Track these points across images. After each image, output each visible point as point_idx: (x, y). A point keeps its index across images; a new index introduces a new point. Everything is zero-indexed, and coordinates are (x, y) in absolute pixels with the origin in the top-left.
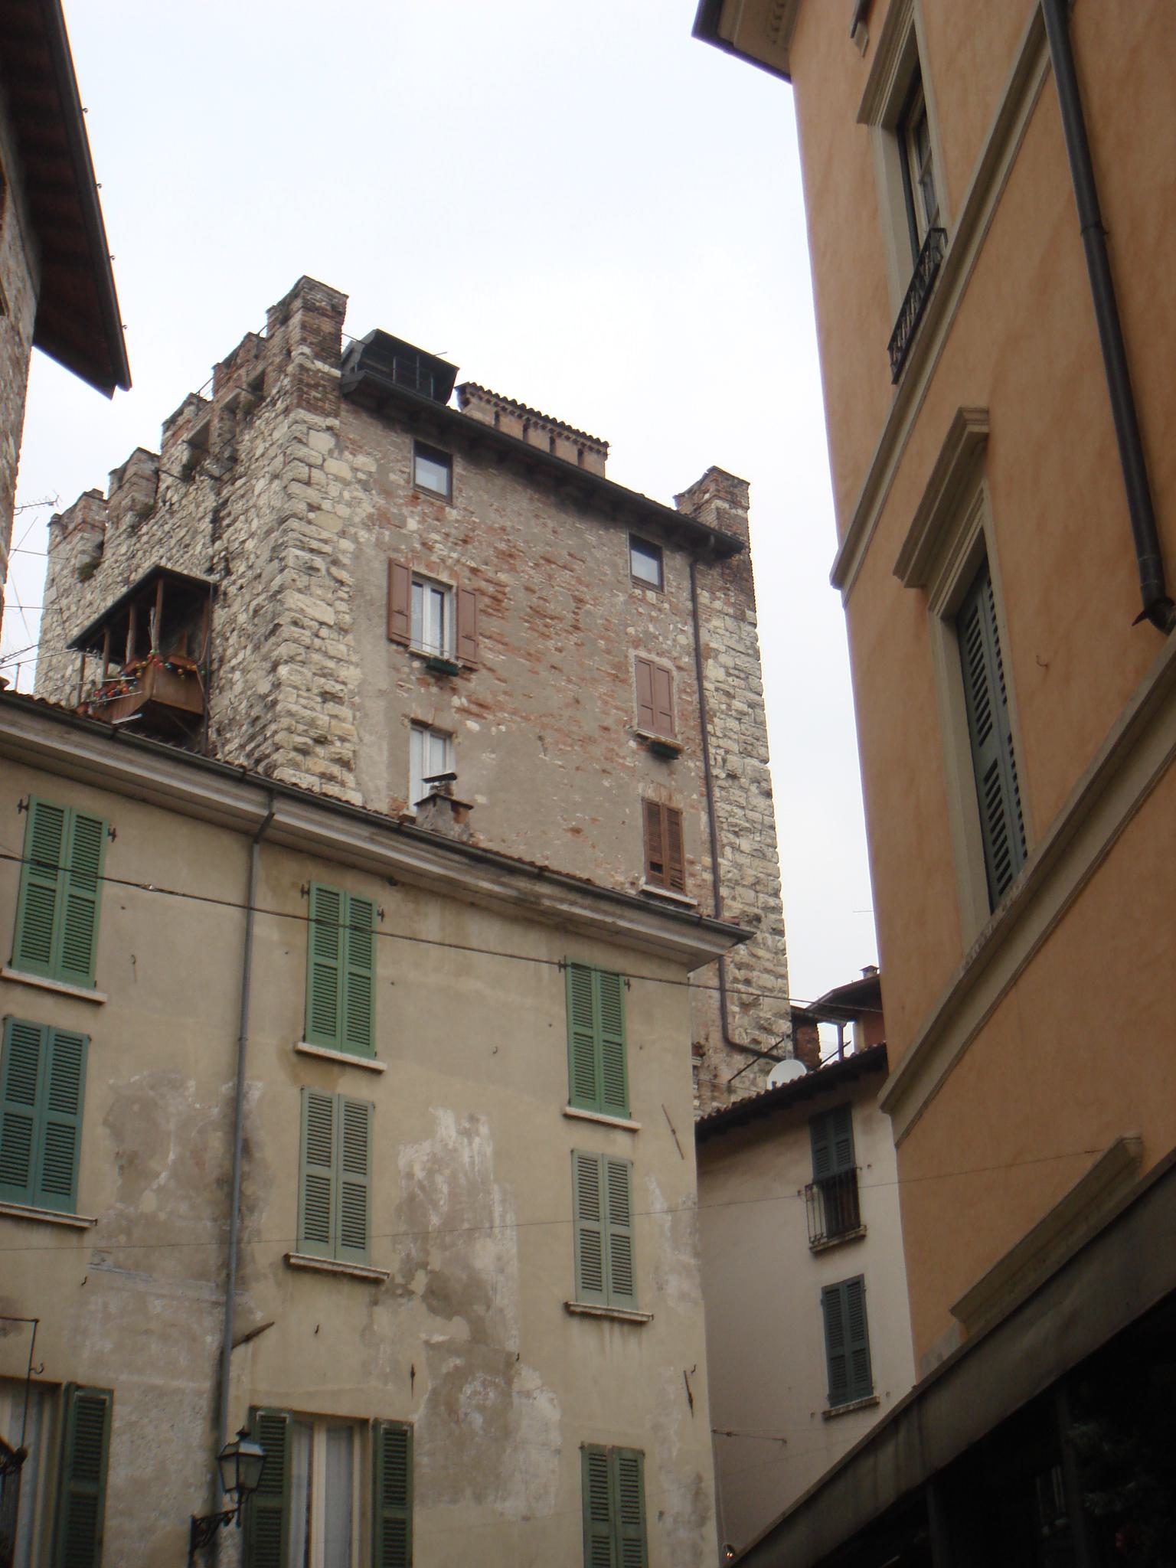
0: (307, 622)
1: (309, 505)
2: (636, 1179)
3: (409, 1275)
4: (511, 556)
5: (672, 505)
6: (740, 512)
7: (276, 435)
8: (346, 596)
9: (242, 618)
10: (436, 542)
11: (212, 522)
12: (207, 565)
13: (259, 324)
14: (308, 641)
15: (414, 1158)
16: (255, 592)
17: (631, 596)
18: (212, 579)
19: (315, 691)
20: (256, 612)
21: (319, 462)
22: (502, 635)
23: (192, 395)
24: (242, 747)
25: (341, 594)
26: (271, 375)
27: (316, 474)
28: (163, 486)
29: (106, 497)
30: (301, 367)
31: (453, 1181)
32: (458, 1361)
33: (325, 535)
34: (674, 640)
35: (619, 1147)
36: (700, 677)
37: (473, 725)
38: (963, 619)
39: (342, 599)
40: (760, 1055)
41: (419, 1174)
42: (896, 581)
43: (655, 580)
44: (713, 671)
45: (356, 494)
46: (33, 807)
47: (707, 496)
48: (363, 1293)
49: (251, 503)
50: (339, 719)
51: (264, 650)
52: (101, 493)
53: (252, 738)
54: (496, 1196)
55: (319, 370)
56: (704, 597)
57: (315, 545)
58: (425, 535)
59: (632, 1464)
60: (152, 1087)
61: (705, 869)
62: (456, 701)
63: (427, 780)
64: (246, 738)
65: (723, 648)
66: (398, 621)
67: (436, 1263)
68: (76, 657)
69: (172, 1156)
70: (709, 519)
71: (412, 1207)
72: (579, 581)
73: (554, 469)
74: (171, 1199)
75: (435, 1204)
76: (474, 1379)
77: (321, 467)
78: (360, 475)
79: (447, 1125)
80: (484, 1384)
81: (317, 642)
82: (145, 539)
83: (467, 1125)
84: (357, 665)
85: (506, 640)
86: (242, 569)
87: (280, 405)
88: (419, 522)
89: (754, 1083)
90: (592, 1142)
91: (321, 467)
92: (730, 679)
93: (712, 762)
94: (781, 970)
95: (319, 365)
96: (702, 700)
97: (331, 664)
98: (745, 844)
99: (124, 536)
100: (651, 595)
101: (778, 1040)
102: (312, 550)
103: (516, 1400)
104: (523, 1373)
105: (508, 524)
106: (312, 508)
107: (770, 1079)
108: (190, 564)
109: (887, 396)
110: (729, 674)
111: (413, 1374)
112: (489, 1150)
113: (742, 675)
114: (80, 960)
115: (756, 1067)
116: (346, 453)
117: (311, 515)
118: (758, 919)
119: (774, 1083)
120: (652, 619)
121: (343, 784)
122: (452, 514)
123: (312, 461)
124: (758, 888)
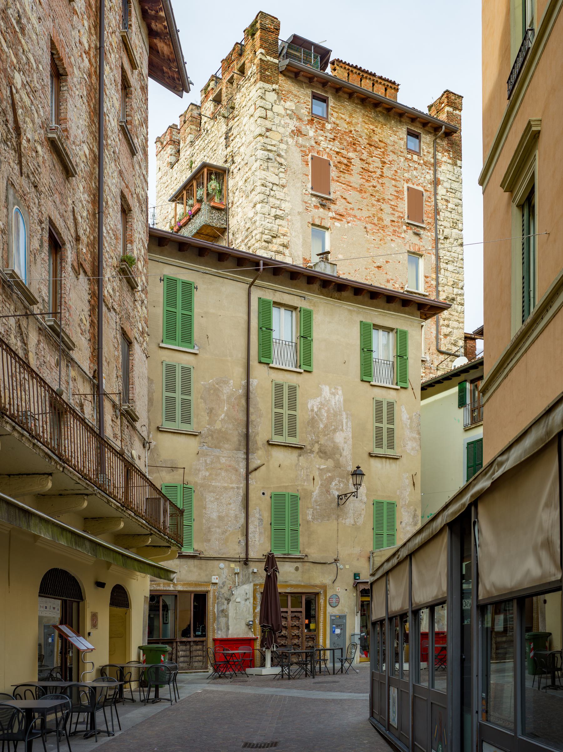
0: (268, 184)
2: (396, 408)
3: (313, 445)
5: (426, 111)
6: (457, 112)
7: (251, 95)
8: (283, 170)
9: (241, 183)
10: (322, 141)
11: (225, 139)
12: (225, 159)
13: (240, 37)
15: (313, 404)
16: (245, 171)
17: (406, 159)
18: (226, 166)
20: (246, 181)
21: (270, 107)
23: (213, 76)
24: (243, 241)
25: (281, 170)
26: (247, 65)
27: (269, 114)
28: (203, 122)
29: (179, 128)
30: (261, 59)
31: (328, 411)
32: (330, 474)
33: (274, 142)
34: (425, 178)
36: (436, 194)
37: (337, 224)
38: (527, 205)
39: (281, 172)
40: (450, 355)
41: (316, 410)
42: (501, 190)
43: (417, 150)
44: (441, 190)
45: (286, 121)
46: (165, 280)
47: (443, 105)
48: (296, 453)
49: (241, 129)
50: (282, 226)
51: (250, 198)
52: (177, 126)
53: (247, 237)
54: (344, 416)
55: (268, 61)
57: (269, 147)
59: (392, 506)
60: (217, 384)
62: (331, 214)
63: (318, 255)
64: (244, 236)
65: (446, 180)
66: (304, 281)
67: (322, 442)
68: (173, 204)
69: (226, 408)
70: (443, 117)
71: (312, 422)
73: (374, 99)
74: (226, 418)
75: (321, 420)
78: (288, 112)
79: (326, 390)
80: (339, 482)
82: (197, 148)
84: (289, 202)
85: (351, 184)
86: (239, 160)
87: (252, 80)
88: (314, 132)
89: (447, 366)
91: (272, 110)
92: (448, 194)
93: (438, 232)
94: (461, 320)
95: (268, 58)
96: (436, 204)
98: (450, 267)
99: (188, 146)
100: (415, 157)
101: (458, 348)
102: (268, 150)
105: (353, 129)
106: (268, 130)
107: (454, 364)
108: (218, 161)
109: (506, 104)
110: (447, 191)
111: (314, 479)
112: (342, 400)
113: (454, 191)
114: (187, 338)
115: (449, 359)
116: (282, 101)
117: (268, 134)
118: (453, 299)
119: (455, 366)
121: (284, 254)
123: (267, 107)
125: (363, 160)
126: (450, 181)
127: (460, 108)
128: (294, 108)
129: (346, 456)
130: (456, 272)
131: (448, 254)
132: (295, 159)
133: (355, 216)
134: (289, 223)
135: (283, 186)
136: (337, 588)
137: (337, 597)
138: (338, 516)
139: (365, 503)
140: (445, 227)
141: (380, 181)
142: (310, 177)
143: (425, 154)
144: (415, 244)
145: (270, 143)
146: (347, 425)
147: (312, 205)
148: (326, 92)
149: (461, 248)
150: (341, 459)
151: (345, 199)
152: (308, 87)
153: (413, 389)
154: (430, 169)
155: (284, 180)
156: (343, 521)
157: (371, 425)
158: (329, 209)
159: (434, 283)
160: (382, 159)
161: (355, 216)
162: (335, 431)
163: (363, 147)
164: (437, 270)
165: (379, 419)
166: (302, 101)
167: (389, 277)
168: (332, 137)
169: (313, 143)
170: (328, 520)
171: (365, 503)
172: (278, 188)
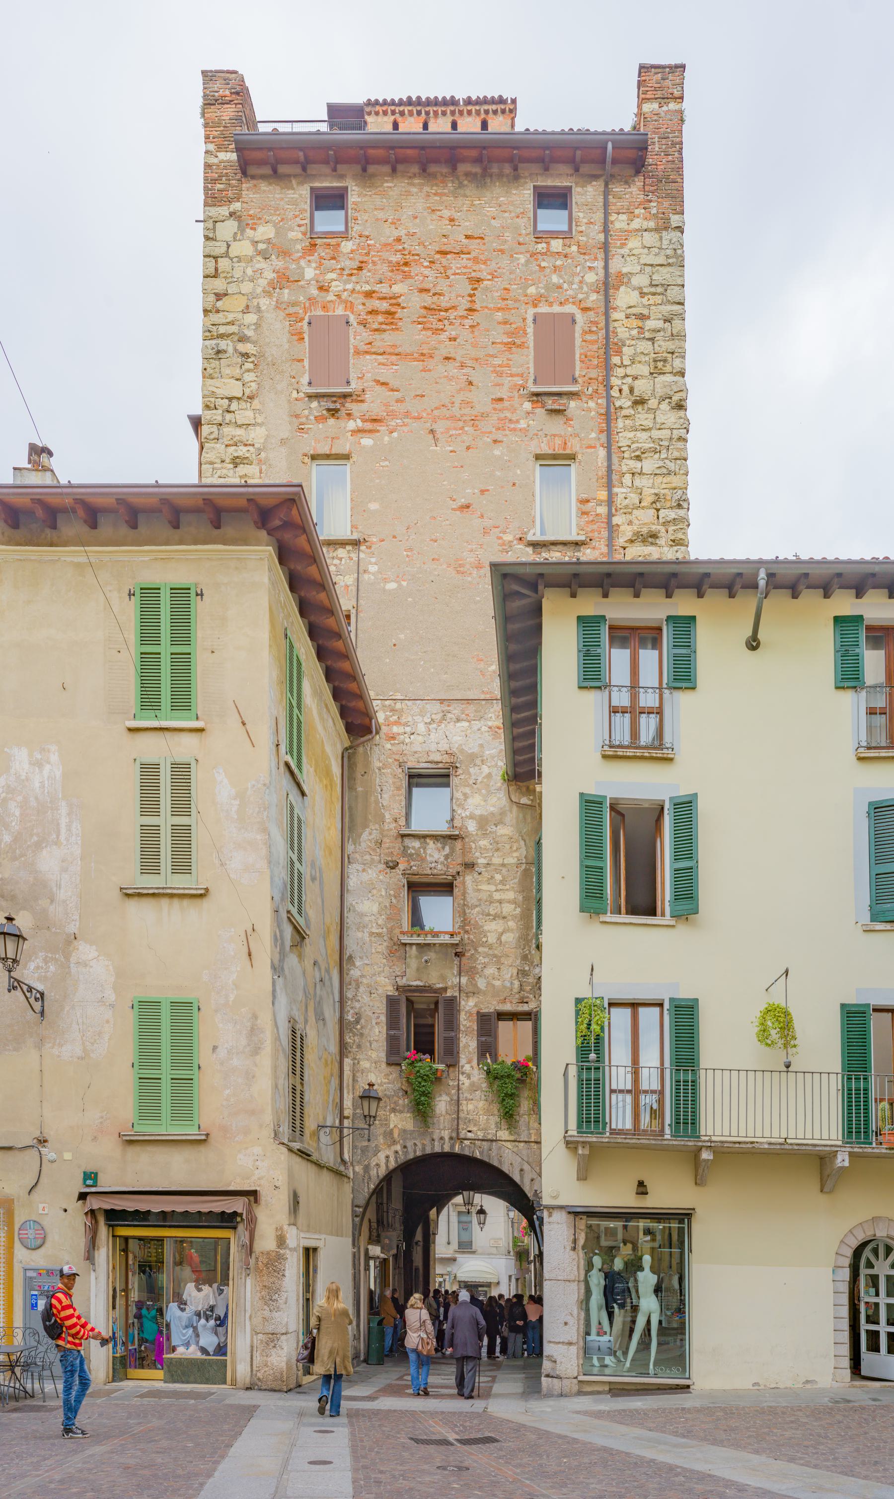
0: (219, 402)
1: (216, 294)
4: (406, 264)
8: (251, 366)
14: (219, 419)
19: (228, 460)
22: (394, 346)
33: (230, 317)
35: (184, 748)
37: (367, 441)
39: (248, 371)
45: (258, 266)
54: (64, 810)
56: (619, 222)
57: (222, 329)
58: (321, 279)
59: (184, 1011)
61: (600, 503)
62: (351, 425)
72: (476, 260)
76: (36, 958)
77: (226, 255)
78: (261, 246)
79: (21, 758)
80: (46, 961)
81: (228, 417)
83: (39, 757)
90: (153, 748)
91: (226, 255)
97: (239, 432)
103: (74, 969)
104: (81, 948)
105: (402, 233)
106: (219, 296)
110: (642, 294)
112: (58, 774)
113: (659, 290)
116: (248, 230)
117: (219, 304)
120: (556, 269)
122: (347, 246)
124: (658, 505)
125: (427, 291)
126: (648, 269)
127: (677, 93)
128: (272, 235)
129: (64, 901)
130: (665, 471)
131: (644, 435)
132: (276, 334)
133: (407, 414)
134: (264, 467)
135: (251, 398)
136: (41, 1206)
137: (38, 1227)
138: (40, 1043)
139: (112, 1006)
140: (635, 378)
141: (468, 322)
142: (306, 363)
143: (583, 228)
144: (554, 435)
145: (224, 321)
146: (69, 829)
147: (312, 418)
148: (342, 177)
149: (681, 413)
150: (51, 908)
151: (383, 384)
152: (301, 183)
153: (244, 724)
154: (596, 259)
155: (253, 384)
156: (55, 1051)
157: (130, 822)
158: (349, 415)
159: (602, 510)
160: (473, 274)
161: (407, 414)
162: (38, 846)
163: (426, 264)
164: (609, 481)
165: (149, 805)
166: (291, 215)
167: (488, 523)
168: (356, 264)
169: (314, 292)
170: (15, 1049)
171: (112, 1006)
172: (243, 405)
